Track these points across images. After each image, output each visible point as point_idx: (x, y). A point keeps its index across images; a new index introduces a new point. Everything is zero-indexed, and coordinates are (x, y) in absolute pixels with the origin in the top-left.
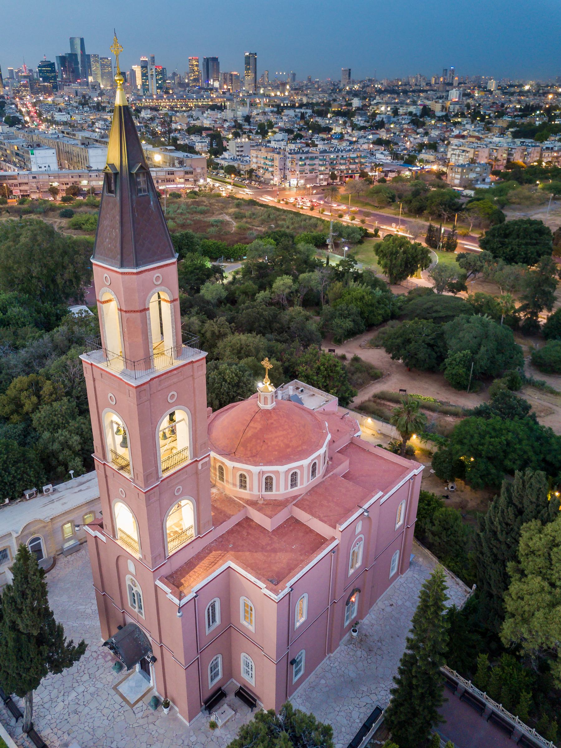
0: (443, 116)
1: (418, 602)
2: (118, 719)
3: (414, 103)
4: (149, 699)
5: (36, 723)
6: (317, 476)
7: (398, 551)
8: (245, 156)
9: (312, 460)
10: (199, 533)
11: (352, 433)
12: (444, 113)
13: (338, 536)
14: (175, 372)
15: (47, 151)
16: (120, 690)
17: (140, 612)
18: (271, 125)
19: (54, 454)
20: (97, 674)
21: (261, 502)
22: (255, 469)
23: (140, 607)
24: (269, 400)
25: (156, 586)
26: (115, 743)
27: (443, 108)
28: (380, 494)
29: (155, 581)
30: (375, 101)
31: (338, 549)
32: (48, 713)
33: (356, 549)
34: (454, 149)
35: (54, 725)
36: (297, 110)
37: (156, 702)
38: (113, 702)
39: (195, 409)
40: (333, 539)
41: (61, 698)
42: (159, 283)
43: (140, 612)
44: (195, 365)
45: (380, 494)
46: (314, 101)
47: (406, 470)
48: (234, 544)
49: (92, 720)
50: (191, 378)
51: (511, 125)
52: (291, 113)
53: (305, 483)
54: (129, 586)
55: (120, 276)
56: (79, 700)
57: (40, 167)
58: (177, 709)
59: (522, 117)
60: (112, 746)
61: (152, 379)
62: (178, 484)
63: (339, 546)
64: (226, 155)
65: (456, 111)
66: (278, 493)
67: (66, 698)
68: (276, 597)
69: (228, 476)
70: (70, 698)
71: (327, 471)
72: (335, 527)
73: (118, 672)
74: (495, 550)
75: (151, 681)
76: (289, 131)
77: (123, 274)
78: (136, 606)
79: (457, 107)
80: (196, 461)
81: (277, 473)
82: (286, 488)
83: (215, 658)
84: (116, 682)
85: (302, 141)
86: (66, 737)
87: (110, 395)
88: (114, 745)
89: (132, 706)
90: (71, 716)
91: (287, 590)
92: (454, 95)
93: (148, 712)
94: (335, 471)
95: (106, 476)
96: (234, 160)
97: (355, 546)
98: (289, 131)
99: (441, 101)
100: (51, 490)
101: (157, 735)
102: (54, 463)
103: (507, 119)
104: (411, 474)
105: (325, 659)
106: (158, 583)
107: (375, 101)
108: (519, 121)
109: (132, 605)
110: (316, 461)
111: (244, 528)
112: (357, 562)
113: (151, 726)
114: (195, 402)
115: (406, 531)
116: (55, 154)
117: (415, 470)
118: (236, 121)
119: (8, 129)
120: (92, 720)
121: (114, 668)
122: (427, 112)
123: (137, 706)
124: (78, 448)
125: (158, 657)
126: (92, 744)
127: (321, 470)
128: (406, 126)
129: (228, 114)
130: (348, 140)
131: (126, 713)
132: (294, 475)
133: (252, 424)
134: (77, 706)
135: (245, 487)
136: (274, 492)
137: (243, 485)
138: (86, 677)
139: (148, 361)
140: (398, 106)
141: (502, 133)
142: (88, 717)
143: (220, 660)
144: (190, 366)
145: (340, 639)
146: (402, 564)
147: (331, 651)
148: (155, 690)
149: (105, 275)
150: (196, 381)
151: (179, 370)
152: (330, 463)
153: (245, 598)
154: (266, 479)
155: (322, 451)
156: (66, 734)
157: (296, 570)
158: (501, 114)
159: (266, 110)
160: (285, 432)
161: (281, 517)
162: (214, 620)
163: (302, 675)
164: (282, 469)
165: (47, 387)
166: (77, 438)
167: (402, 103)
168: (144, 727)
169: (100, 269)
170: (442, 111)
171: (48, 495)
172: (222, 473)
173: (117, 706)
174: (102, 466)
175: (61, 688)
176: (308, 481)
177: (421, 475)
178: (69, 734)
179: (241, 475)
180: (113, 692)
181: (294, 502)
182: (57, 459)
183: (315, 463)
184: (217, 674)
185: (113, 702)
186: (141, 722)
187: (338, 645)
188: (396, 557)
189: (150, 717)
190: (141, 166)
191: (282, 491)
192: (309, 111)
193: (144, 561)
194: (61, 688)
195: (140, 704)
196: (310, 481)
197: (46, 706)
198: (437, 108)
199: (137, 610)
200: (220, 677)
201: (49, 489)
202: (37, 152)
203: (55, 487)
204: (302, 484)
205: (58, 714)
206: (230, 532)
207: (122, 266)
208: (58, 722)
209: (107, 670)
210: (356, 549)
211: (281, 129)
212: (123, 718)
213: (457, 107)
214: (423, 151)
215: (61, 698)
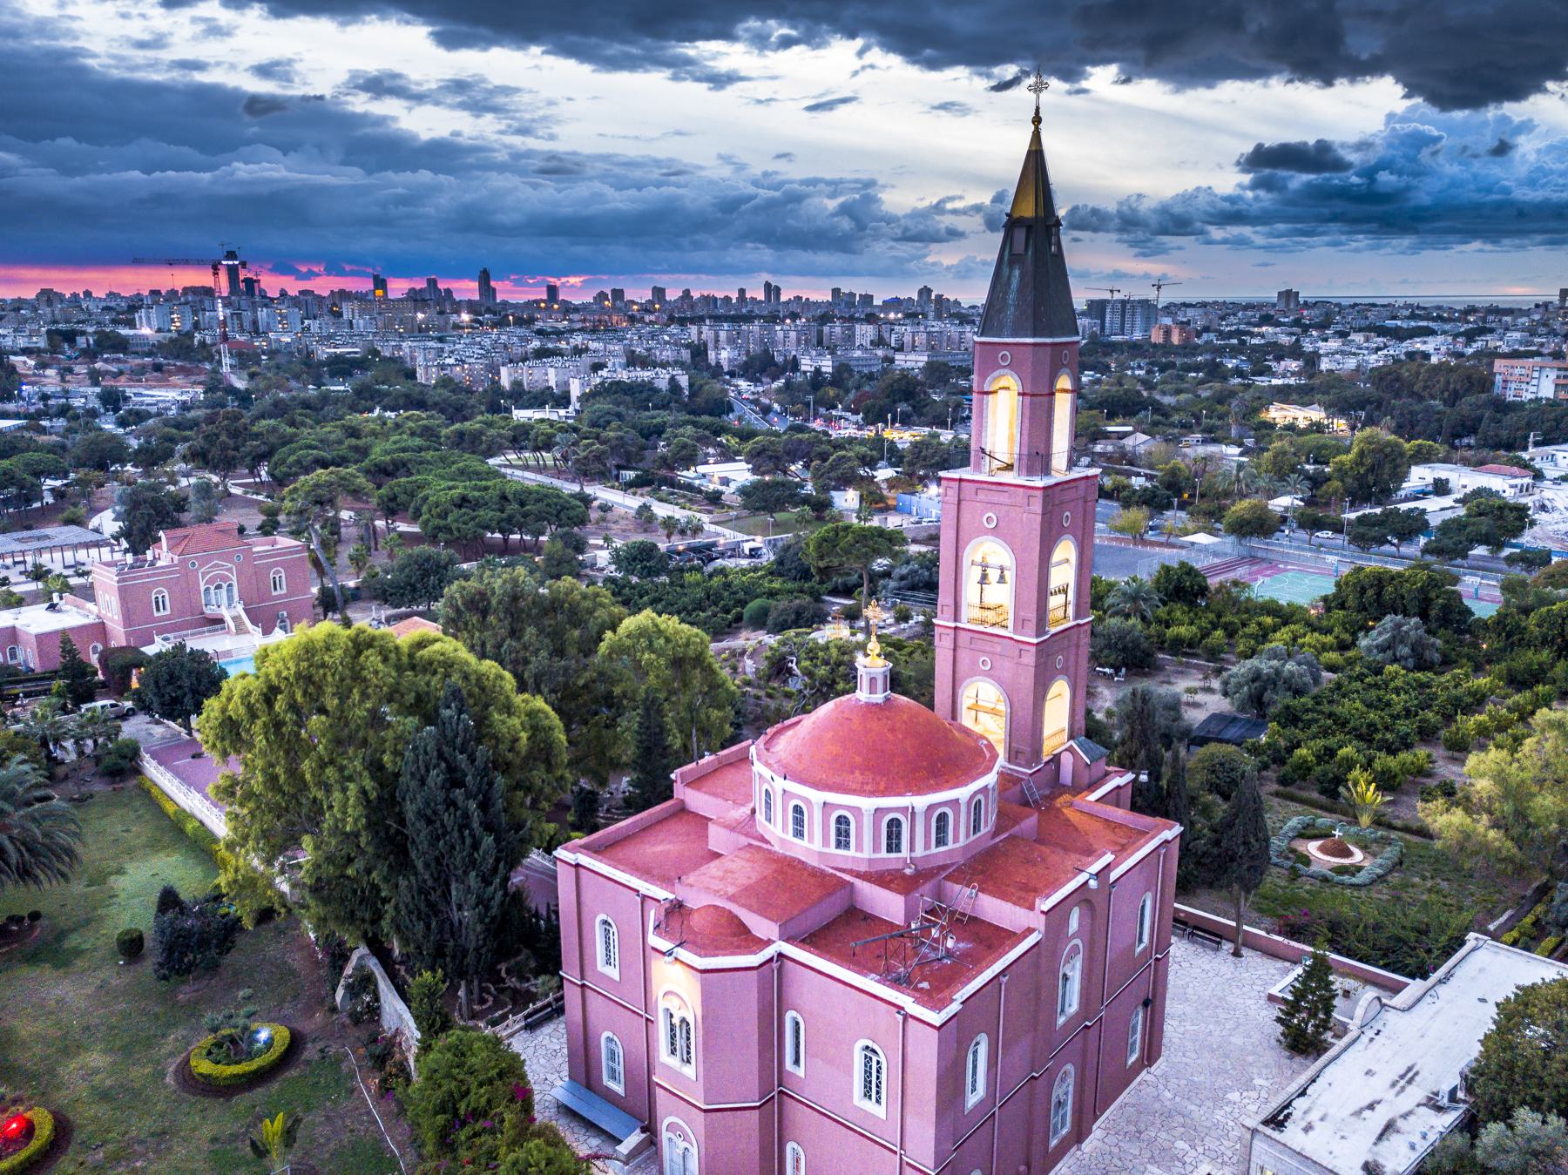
1: (1424, 253)
7: (1069, 1067)
9: (975, 793)
13: (1039, 922)
22: (868, 804)
40: (1030, 931)
53: (960, 840)
63: (1043, 946)
69: (814, 821)
72: (1031, 908)
82: (927, 847)
91: (955, 1007)
110: (980, 796)
132: (942, 818)
135: (847, 846)
137: (843, 839)
139: (1046, 470)
153: (795, 1145)
164: (920, 802)
172: (799, 822)
176: (968, 835)
179: (840, 820)
196: (973, 838)
204: (956, 840)
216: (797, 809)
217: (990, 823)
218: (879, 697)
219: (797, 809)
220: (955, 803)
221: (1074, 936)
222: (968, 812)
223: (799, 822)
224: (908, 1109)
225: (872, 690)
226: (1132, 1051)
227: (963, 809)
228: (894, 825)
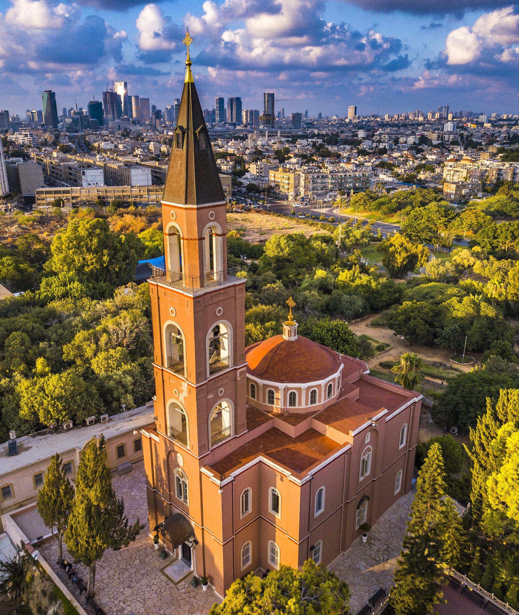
0: (439, 144)
2: (164, 594)
3: (413, 134)
4: (190, 579)
5: (97, 593)
6: (333, 397)
7: (401, 471)
8: (264, 177)
9: (329, 381)
10: (236, 433)
11: (361, 370)
12: (440, 142)
14: (222, 291)
15: (96, 171)
16: (166, 572)
17: (185, 501)
18: (287, 151)
19: (110, 391)
20: (147, 560)
21: (286, 415)
23: (186, 498)
24: (293, 334)
25: (201, 472)
26: (162, 610)
27: (439, 137)
28: (386, 411)
29: (200, 468)
30: (378, 132)
31: (351, 453)
32: (106, 586)
33: (365, 457)
34: (450, 170)
35: (112, 595)
36: (310, 140)
37: (196, 583)
38: (160, 581)
39: (236, 325)
40: (347, 443)
41: (117, 576)
42: (212, 219)
43: (185, 501)
44: (238, 288)
45: (386, 411)
46: (324, 133)
47: (406, 399)
48: (264, 446)
49: (142, 593)
50: (234, 299)
51: (500, 151)
52: (304, 142)
53: (322, 401)
54: (177, 477)
55: (184, 211)
56: (132, 578)
57: (90, 184)
58: (214, 588)
59: (510, 144)
60: (160, 612)
61: (205, 294)
62: (221, 386)
63: (352, 450)
64: (247, 175)
65: (451, 140)
66: (300, 407)
67: (121, 576)
68: (300, 481)
70: (124, 577)
71: (341, 395)
72: (348, 434)
73: (163, 559)
74: (483, 462)
75: (192, 566)
76: (303, 157)
77: (186, 209)
78: (183, 497)
79: (452, 136)
80: (236, 369)
81: (299, 389)
82: (307, 404)
83: (246, 543)
84: (162, 566)
85: (314, 164)
86: (122, 604)
87: (172, 308)
88: (162, 612)
89: (176, 584)
90: (126, 589)
91: (308, 478)
92: (449, 127)
93: (190, 589)
94: (347, 396)
95: (163, 381)
96: (254, 179)
97: (364, 455)
98: (303, 157)
99: (437, 132)
100: (107, 419)
101: (197, 606)
102: (109, 398)
103: (497, 146)
104: (412, 401)
105: (339, 556)
106: (203, 470)
107: (378, 132)
108: (507, 147)
109: (178, 496)
110: (331, 383)
111: (272, 434)
112: (366, 472)
113: (192, 600)
114: (236, 319)
115: (409, 454)
116: (102, 174)
117: (415, 399)
118: (256, 148)
119: (62, 155)
120: (142, 593)
121: (160, 556)
122: (424, 140)
123: (180, 584)
124: (131, 388)
125: (200, 540)
126: (143, 610)
127: (336, 393)
128: (405, 152)
129: (249, 143)
130: (354, 163)
131: (171, 590)
132: (314, 392)
133: (278, 352)
134: (130, 583)
136: (297, 407)
138: (137, 562)
140: (399, 136)
141: (493, 156)
142: (140, 591)
143: (250, 546)
144: (233, 288)
145: (352, 542)
146: (406, 478)
147: (344, 549)
148: (195, 573)
149: (172, 212)
150: (237, 301)
151: (225, 290)
152: (343, 389)
154: (291, 394)
155: (337, 375)
156: (122, 603)
157: (316, 464)
158: (490, 143)
159: (283, 139)
160: (306, 359)
161: (302, 427)
162: (247, 509)
163: (322, 513)
164: (304, 386)
165: (104, 339)
166: (129, 378)
167: (402, 134)
168: (187, 600)
169: (167, 208)
170: (438, 140)
171: (104, 423)
172: (253, 392)
173: (163, 584)
174: (161, 372)
175: (117, 569)
176: (325, 400)
177: (420, 402)
178: (124, 603)
180: (160, 574)
181: (314, 416)
182: (112, 395)
183: (331, 385)
184: (247, 560)
185: (160, 581)
186: (184, 596)
187: (350, 546)
188: (400, 476)
189: (191, 593)
190: (202, 128)
191: (303, 406)
192: (320, 141)
193: (192, 451)
194: (117, 569)
195: (183, 583)
196: (327, 400)
197: (105, 581)
198: (433, 137)
199: (182, 500)
200: (250, 563)
201: (105, 418)
202: (88, 172)
203: (111, 417)
204: (320, 401)
205: (115, 588)
206: (261, 437)
207: (186, 203)
208: (115, 593)
209: (155, 558)
210: (365, 457)
211: (296, 156)
212: (168, 592)
213: (452, 136)
214: (422, 172)
215: (117, 576)
216: (253, 386)
217: (336, 394)
218: (293, 338)
219: (253, 386)
220: (319, 386)
221: (368, 444)
222: (325, 390)
223: (253, 392)
224: (308, 501)
225: (290, 335)
226: (397, 488)
227: (323, 389)
228: (293, 395)
